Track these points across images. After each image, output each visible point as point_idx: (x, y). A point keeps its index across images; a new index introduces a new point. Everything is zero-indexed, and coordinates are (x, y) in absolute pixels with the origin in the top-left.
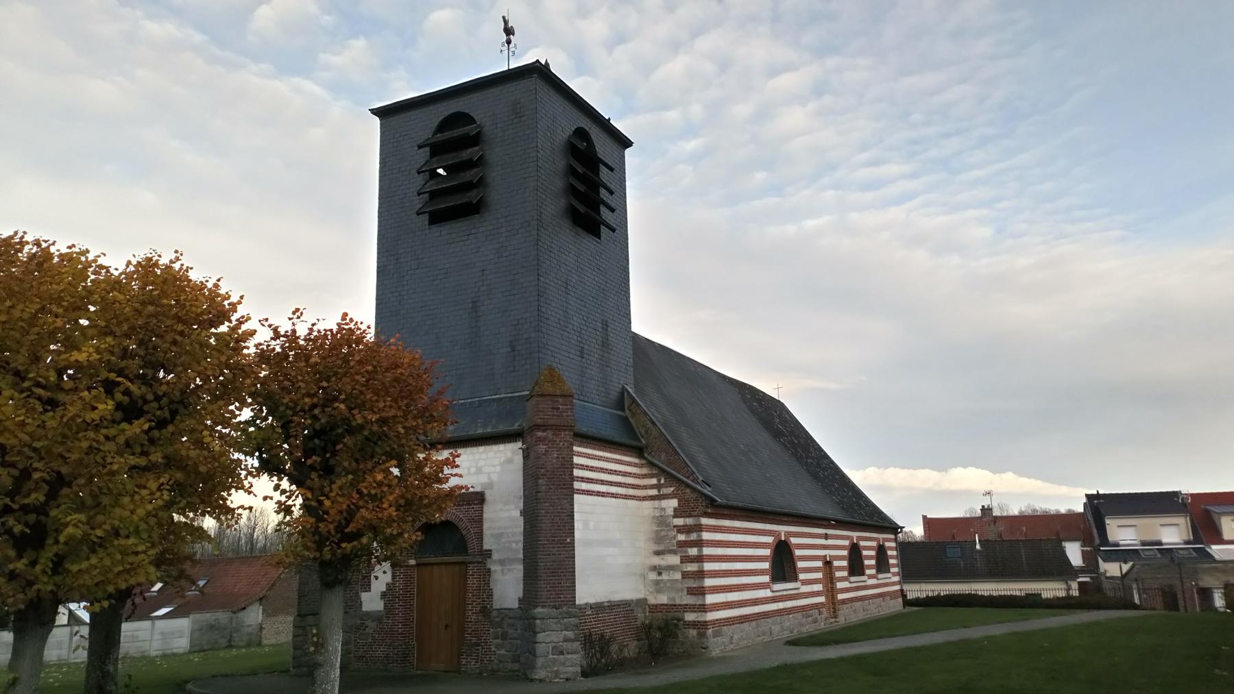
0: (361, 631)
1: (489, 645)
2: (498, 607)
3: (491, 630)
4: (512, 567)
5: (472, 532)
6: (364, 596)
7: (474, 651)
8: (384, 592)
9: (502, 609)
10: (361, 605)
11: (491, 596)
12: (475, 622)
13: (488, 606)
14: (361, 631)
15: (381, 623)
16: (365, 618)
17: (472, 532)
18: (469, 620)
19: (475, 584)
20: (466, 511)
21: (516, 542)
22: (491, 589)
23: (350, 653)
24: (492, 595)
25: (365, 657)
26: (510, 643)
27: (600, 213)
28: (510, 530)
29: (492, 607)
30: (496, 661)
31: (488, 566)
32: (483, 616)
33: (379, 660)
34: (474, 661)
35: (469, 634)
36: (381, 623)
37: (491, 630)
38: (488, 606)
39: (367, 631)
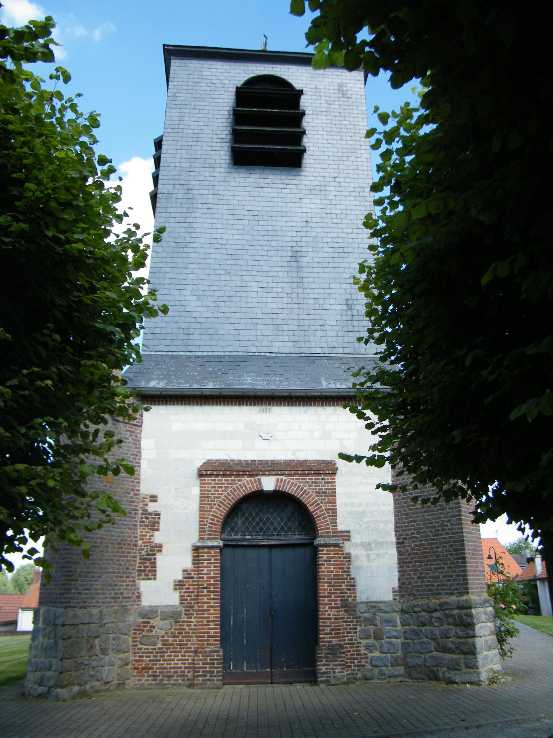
0: (144, 633)
1: (357, 647)
2: (364, 600)
4: (381, 552)
5: (324, 508)
6: (144, 586)
8: (180, 581)
10: (139, 597)
11: (352, 586)
12: (335, 619)
13: (350, 599)
14: (144, 633)
15: (177, 622)
18: (326, 616)
19: (332, 572)
20: (313, 482)
21: (386, 522)
22: (353, 579)
23: (127, 664)
24: (354, 586)
26: (388, 642)
28: (376, 508)
29: (355, 600)
30: (368, 666)
31: (347, 550)
32: (345, 611)
33: (175, 672)
34: (339, 667)
35: (326, 634)
36: (177, 622)
37: (359, 628)
38: (350, 599)
39: (153, 633)
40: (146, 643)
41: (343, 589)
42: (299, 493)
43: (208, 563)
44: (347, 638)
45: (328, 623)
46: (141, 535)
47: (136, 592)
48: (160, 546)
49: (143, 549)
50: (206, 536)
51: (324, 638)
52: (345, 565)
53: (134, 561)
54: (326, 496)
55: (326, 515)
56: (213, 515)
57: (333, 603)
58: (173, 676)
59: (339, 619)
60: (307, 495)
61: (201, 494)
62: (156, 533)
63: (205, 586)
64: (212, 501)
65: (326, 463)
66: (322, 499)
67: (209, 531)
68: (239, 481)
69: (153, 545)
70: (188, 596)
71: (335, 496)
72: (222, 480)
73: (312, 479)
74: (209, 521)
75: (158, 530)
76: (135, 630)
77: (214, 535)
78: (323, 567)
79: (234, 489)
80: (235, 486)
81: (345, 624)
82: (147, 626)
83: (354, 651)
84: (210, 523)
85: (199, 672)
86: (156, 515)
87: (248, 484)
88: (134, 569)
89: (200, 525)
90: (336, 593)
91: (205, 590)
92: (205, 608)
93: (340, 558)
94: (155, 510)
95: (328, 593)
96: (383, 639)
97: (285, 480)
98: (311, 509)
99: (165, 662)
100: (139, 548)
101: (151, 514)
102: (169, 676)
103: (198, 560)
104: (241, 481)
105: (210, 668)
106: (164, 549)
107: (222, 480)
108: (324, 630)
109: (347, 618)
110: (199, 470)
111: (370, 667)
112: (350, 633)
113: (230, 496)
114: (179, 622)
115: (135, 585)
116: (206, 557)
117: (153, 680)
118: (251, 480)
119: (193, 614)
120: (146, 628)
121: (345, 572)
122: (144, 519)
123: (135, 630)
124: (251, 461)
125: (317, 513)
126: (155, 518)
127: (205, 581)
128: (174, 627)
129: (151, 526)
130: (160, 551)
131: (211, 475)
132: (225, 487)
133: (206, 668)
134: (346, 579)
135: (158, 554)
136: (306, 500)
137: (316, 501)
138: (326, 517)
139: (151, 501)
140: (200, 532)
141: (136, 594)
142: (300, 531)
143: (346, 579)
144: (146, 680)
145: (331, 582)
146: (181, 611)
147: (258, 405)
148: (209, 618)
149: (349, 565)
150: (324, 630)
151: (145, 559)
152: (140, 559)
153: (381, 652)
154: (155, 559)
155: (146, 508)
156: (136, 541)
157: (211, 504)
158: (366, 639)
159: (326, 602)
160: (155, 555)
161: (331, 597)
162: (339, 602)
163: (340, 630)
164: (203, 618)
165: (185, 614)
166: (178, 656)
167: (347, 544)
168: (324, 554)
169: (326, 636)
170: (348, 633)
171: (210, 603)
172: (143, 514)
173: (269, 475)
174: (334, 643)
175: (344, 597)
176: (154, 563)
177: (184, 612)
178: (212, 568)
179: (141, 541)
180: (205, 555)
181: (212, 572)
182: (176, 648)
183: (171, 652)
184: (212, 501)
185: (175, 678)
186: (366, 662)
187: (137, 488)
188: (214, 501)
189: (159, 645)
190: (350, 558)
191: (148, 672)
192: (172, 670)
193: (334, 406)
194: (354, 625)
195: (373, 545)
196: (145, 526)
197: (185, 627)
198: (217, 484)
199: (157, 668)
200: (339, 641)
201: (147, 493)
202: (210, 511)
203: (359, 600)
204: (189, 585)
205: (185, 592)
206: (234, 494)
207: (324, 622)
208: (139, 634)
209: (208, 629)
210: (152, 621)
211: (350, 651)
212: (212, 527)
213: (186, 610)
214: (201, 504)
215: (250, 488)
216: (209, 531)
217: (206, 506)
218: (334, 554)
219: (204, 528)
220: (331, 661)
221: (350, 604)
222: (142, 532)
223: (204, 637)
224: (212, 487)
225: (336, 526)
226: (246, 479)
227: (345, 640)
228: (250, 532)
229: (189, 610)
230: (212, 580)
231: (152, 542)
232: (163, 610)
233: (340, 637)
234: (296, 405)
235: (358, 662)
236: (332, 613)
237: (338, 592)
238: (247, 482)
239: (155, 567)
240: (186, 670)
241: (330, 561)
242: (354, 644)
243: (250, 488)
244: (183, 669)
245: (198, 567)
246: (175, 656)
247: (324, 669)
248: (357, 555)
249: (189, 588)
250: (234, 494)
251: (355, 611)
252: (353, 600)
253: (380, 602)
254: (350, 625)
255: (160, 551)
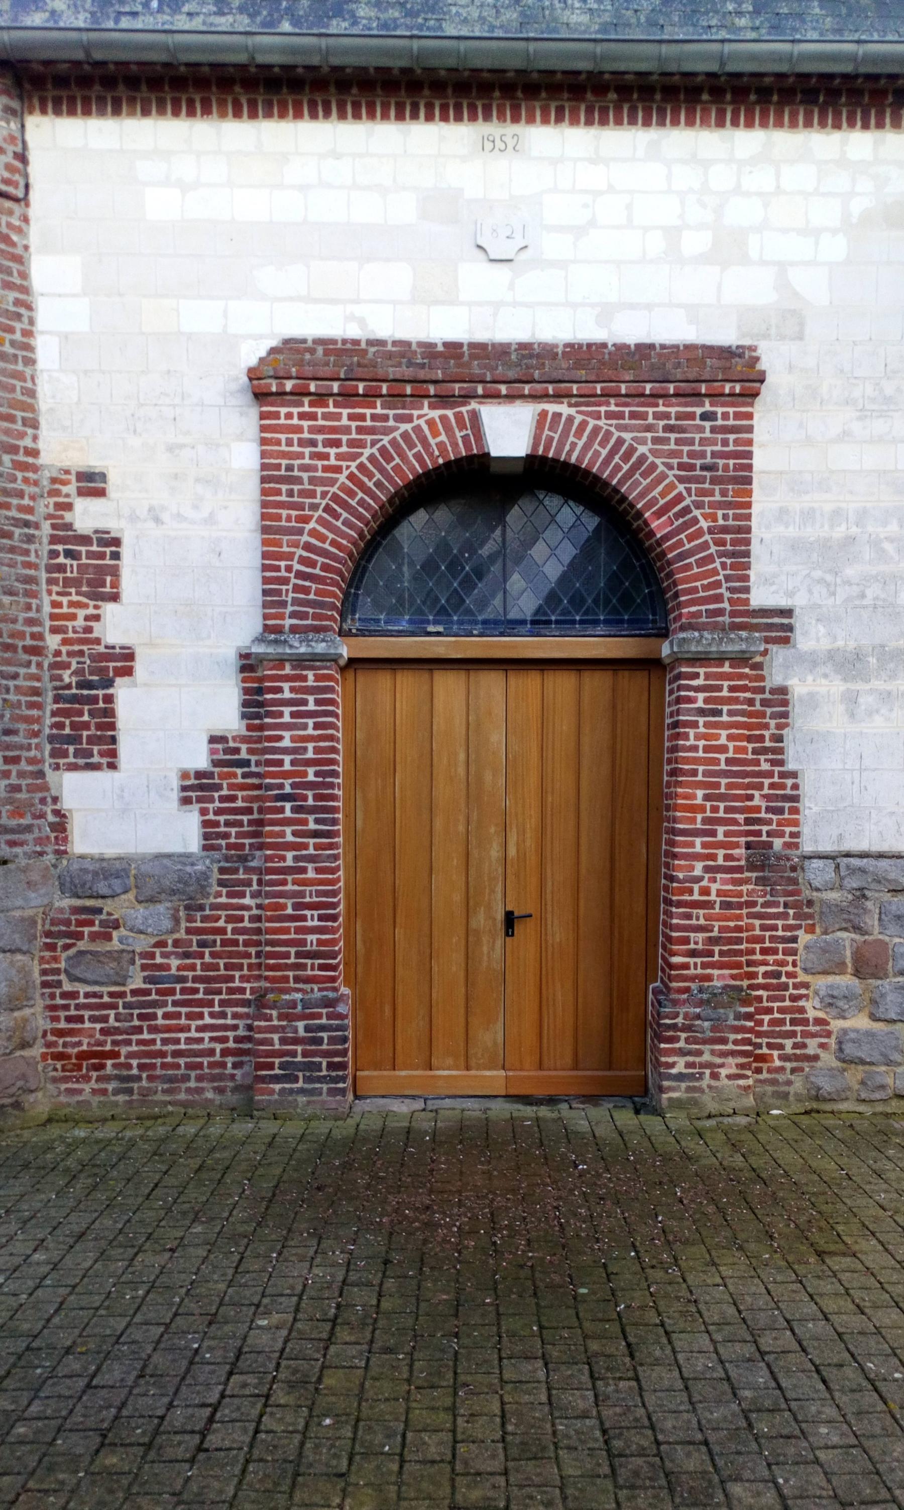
0: (82, 945)
1: (794, 998)
2: (827, 847)
3: (804, 938)
5: (704, 524)
7: (732, 1022)
8: (199, 775)
9: (848, 855)
12: (726, 905)
14: (82, 945)
16: (102, 888)
17: (704, 524)
18: (696, 897)
19: (723, 749)
20: (669, 429)
22: (794, 775)
23: (25, 1045)
24: (795, 799)
25: (115, 1055)
27: (505, 517)
29: (796, 846)
30: (828, 1059)
31: (775, 677)
32: (759, 881)
34: (731, 1060)
35: (693, 953)
37: (804, 938)
38: (778, 843)
39: (115, 944)
40: (89, 976)
41: (757, 809)
42: (618, 468)
43: (293, 715)
44: (762, 969)
45: (700, 917)
46: (53, 617)
47: (48, 810)
48: (129, 656)
49: (67, 666)
50: (288, 622)
51: (686, 966)
52: (766, 726)
53: (32, 705)
54: (714, 481)
55: (713, 549)
56: (308, 547)
57: (721, 853)
58: (186, 1078)
59: (740, 906)
60: (645, 475)
61: (264, 467)
62: (109, 609)
63: (288, 790)
64: (302, 493)
65: (726, 354)
66: (702, 493)
67: (295, 602)
68: (399, 419)
69: (101, 649)
70: (228, 824)
71: (748, 481)
72: (338, 417)
73: (667, 416)
74: (297, 567)
75: (115, 598)
76: (48, 934)
77: (316, 617)
78: (692, 732)
79: (383, 451)
80: (386, 440)
81: (757, 923)
82: (91, 923)
83: (781, 1010)
84: (300, 575)
85: (271, 1066)
86: (103, 542)
87: (436, 434)
88: (36, 734)
89: (266, 580)
90: (735, 822)
91: (288, 806)
92: (289, 862)
93: (751, 702)
94: (101, 525)
95: (705, 821)
96: (886, 976)
97: (570, 419)
98: (659, 526)
99: (158, 1037)
100: (51, 659)
101: (85, 540)
102: (171, 1080)
103: (261, 704)
104: (409, 419)
105: (305, 1054)
106: (139, 666)
107: (338, 417)
108: (686, 941)
109: (766, 905)
110: (254, 375)
111: (836, 1064)
112: (775, 951)
113: (370, 476)
114: (201, 908)
115: (45, 788)
116: (287, 695)
117: (116, 1092)
118: (443, 418)
119: (249, 883)
120: (86, 930)
121: (765, 751)
122: (61, 560)
123: (48, 934)
124: (446, 344)
125: (680, 543)
126: (102, 556)
127: (286, 775)
128: (183, 925)
129: (90, 583)
130: (128, 672)
131: (300, 393)
132: (352, 443)
133: (294, 1054)
134: (770, 774)
135: (118, 680)
136: (642, 495)
137: (679, 498)
138: (710, 559)
139: (81, 493)
140: (265, 605)
141: (51, 818)
142: (614, 610)
143: (770, 774)
144: (94, 1092)
145: (717, 785)
146: (205, 876)
147: (473, 118)
148: (302, 894)
149: (779, 727)
150: (686, 941)
151: (75, 699)
152: (57, 699)
153: (874, 1018)
154: (109, 699)
155: (68, 517)
156: (39, 637)
157: (300, 507)
158: (825, 973)
159: (698, 849)
160: (110, 684)
161: (713, 833)
162: (740, 852)
163: (739, 941)
164: (281, 895)
165: (221, 883)
166: (201, 1016)
167: (779, 654)
168: (697, 689)
169: (691, 961)
170: (764, 951)
171: (305, 846)
172: (54, 540)
173: (511, 397)
174: (717, 983)
175: (758, 833)
176: (110, 713)
177: (216, 875)
178: (310, 731)
179: (58, 638)
180: (286, 686)
181: (310, 746)
182: (196, 991)
183: (175, 1003)
184: (303, 493)
185: (192, 1084)
186: (822, 1046)
187: (27, 442)
188: (312, 494)
189: (137, 982)
190: (785, 703)
191: (102, 1067)
192: (182, 1061)
193: (764, 125)
194: (786, 928)
195: (873, 660)
196: (67, 582)
197: (221, 923)
198: (320, 430)
199: (130, 1055)
200: (733, 977)
201: (66, 464)
202: (300, 532)
203: (808, 847)
204: (231, 787)
205: (218, 812)
206: (382, 470)
207: (689, 917)
208: (67, 947)
209: (298, 930)
210: (108, 906)
211: (769, 1011)
212: (306, 590)
213: (222, 871)
214: (264, 505)
215: (440, 445)
216: (295, 602)
217: (284, 513)
218: (732, 689)
219: (278, 593)
220: (705, 1042)
221: (779, 858)
222: (56, 604)
223: (287, 955)
224: (302, 443)
225: (747, 590)
226: (427, 413)
227: (753, 975)
228: (443, 611)
229: (235, 871)
230: (311, 771)
231: (98, 641)
232: (143, 868)
233: (738, 966)
234: (619, 122)
235: (796, 1046)
236: (714, 887)
237: (740, 817)
238: (431, 423)
239: (112, 726)
240: (230, 1060)
241: (719, 713)
242: (785, 987)
243: (440, 445)
244: (218, 1057)
245: (261, 728)
246: (189, 1016)
247: (680, 1066)
248: (812, 695)
249: (233, 799)
250: (382, 470)
251: (795, 881)
252: (787, 845)
253: (881, 856)
254: (775, 928)
255: (128, 672)
